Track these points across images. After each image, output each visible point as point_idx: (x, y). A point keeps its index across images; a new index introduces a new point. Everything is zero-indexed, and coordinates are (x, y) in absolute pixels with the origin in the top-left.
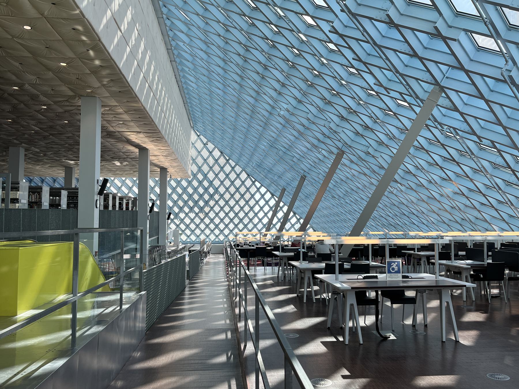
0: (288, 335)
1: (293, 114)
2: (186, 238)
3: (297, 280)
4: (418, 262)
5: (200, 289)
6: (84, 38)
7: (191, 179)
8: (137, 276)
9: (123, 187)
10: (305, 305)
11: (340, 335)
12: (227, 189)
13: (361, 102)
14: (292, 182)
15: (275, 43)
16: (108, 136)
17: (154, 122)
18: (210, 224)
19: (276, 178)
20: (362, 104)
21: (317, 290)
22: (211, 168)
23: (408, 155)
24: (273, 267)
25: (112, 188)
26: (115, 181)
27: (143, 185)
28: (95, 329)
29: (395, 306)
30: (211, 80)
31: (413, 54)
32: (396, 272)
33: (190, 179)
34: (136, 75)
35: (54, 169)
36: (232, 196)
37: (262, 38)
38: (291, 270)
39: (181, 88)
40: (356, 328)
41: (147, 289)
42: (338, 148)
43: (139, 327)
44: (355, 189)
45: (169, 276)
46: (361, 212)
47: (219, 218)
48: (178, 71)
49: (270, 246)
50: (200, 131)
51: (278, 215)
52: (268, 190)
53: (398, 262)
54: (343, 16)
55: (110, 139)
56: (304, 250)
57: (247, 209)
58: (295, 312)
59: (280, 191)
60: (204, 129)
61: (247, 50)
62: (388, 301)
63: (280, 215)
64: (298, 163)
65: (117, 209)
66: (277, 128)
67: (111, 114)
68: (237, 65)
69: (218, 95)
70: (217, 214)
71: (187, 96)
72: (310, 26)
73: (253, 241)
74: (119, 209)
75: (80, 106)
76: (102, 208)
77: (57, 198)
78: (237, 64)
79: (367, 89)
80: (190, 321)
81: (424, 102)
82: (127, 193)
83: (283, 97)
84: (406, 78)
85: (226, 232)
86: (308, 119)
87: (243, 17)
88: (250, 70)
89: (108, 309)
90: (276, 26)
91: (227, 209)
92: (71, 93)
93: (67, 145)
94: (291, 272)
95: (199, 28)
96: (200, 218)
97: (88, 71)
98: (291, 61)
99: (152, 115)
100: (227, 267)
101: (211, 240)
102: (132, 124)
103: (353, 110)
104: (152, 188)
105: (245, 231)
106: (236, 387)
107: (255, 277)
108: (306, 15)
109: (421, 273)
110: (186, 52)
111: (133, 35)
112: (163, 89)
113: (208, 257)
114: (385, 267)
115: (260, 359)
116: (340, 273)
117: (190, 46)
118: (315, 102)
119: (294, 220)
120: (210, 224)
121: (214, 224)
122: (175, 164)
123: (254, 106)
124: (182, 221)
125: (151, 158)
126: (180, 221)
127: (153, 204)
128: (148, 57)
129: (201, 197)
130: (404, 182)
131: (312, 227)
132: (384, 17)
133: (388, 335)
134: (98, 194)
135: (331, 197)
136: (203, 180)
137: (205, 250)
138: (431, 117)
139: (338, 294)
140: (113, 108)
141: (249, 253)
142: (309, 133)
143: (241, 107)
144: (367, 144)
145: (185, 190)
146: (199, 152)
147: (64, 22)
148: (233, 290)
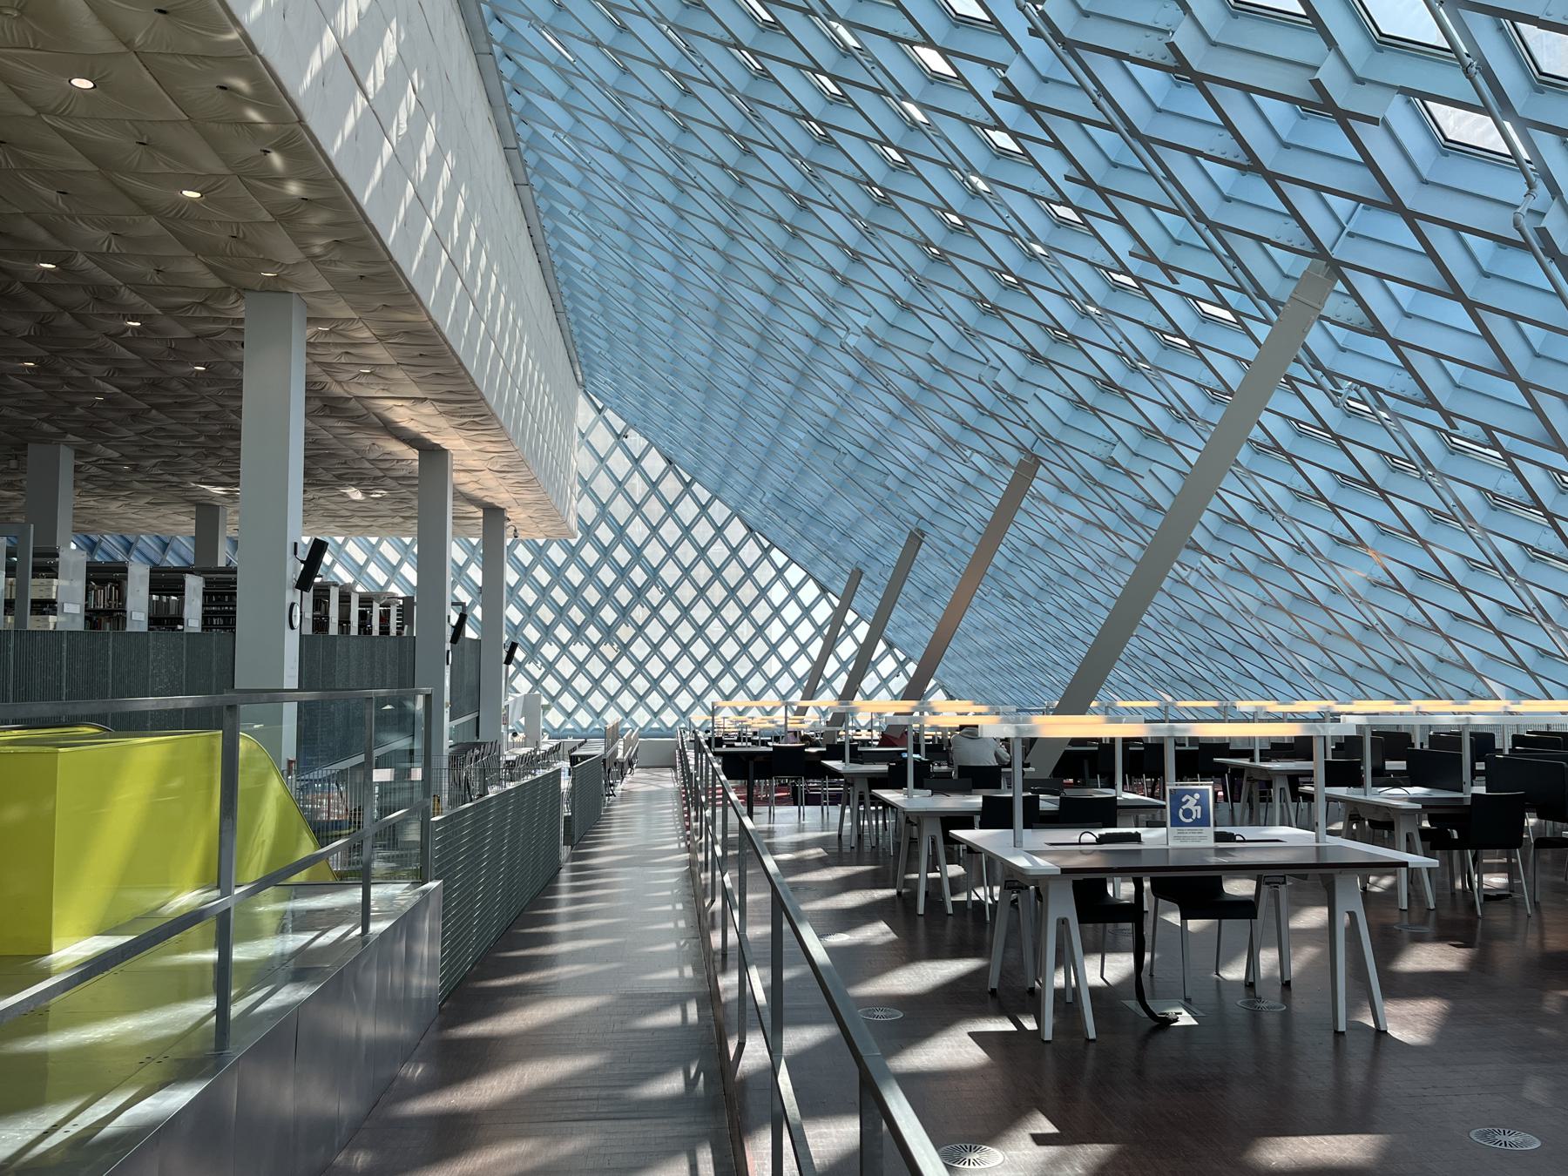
0: (870, 1013)
1: (884, 345)
2: (562, 718)
3: (897, 845)
4: (1262, 793)
5: (603, 873)
6: (254, 115)
7: (577, 540)
8: (413, 834)
9: (372, 565)
10: (921, 921)
11: (1026, 1013)
12: (686, 572)
13: (1091, 309)
14: (883, 551)
15: (830, 131)
16: (328, 411)
17: (465, 369)
18: (633, 676)
19: (833, 538)
20: (1093, 315)
21: (959, 876)
22: (637, 508)
23: (1234, 468)
24: (825, 807)
25: (338, 569)
26: (347, 549)
27: (431, 560)
28: (288, 995)
29: (1193, 925)
30: (639, 241)
31: (1249, 163)
32: (1197, 823)
33: (574, 542)
34: (411, 227)
35: (163, 510)
36: (702, 592)
37: (793, 115)
38: (880, 817)
39: (547, 265)
40: (1076, 992)
41: (445, 873)
42: (1021, 448)
43: (420, 988)
44: (1071, 570)
45: (509, 836)
46: (1091, 640)
47: (663, 658)
48: (538, 216)
49: (816, 745)
50: (604, 395)
51: (839, 650)
52: (809, 575)
53: (1203, 793)
54: (1037, 49)
55: (331, 420)
56: (917, 756)
57: (745, 631)
58: (892, 942)
59: (846, 577)
60: (616, 390)
61: (747, 152)
62: (1173, 910)
63: (847, 649)
64: (900, 493)
65: (354, 631)
66: (836, 388)
67: (336, 345)
68: (717, 196)
69: (659, 286)
70: (655, 648)
71: (564, 290)
72: (937, 78)
73: (764, 729)
74: (359, 633)
75: (241, 321)
76: (308, 630)
77: (173, 598)
78: (715, 192)
79: (1107, 270)
80: (574, 971)
81: (1281, 308)
82: (382, 584)
83: (856, 294)
84: (1226, 235)
85: (684, 700)
86: (931, 361)
87: (735, 52)
88: (755, 211)
89: (327, 934)
90: (834, 79)
91: (685, 632)
92: (214, 282)
93: (202, 439)
94: (880, 822)
95: (601, 84)
96: (603, 658)
97: (265, 216)
98: (878, 183)
99: (460, 348)
100: (686, 809)
101: (637, 726)
102: (399, 374)
103: (1065, 332)
104: (461, 570)
105: (741, 700)
106: (712, 1169)
107: (769, 838)
108: (923, 45)
109: (1273, 824)
110: (563, 158)
111: (403, 105)
112: (493, 270)
113: (628, 778)
114: (1164, 807)
115: (787, 1085)
116: (1026, 826)
117: (575, 139)
118: (950, 309)
119: (887, 666)
120: (633, 676)
121: (648, 676)
122: (529, 497)
123: (766, 321)
124: (550, 667)
125: (457, 478)
126: (543, 669)
127: (463, 618)
128: (446, 173)
129: (607, 596)
130: (1221, 551)
131: (943, 687)
132: (1159, 53)
133: (1171, 1012)
134: (297, 587)
135: (1000, 596)
136: (613, 545)
137: (620, 755)
138: (1301, 354)
139: (1022, 888)
140: (340, 328)
141: (751, 764)
142: (932, 401)
143: (728, 323)
144: (1109, 435)
145: (558, 573)
146: (602, 460)
147: (194, 67)
148: (702, 876)
